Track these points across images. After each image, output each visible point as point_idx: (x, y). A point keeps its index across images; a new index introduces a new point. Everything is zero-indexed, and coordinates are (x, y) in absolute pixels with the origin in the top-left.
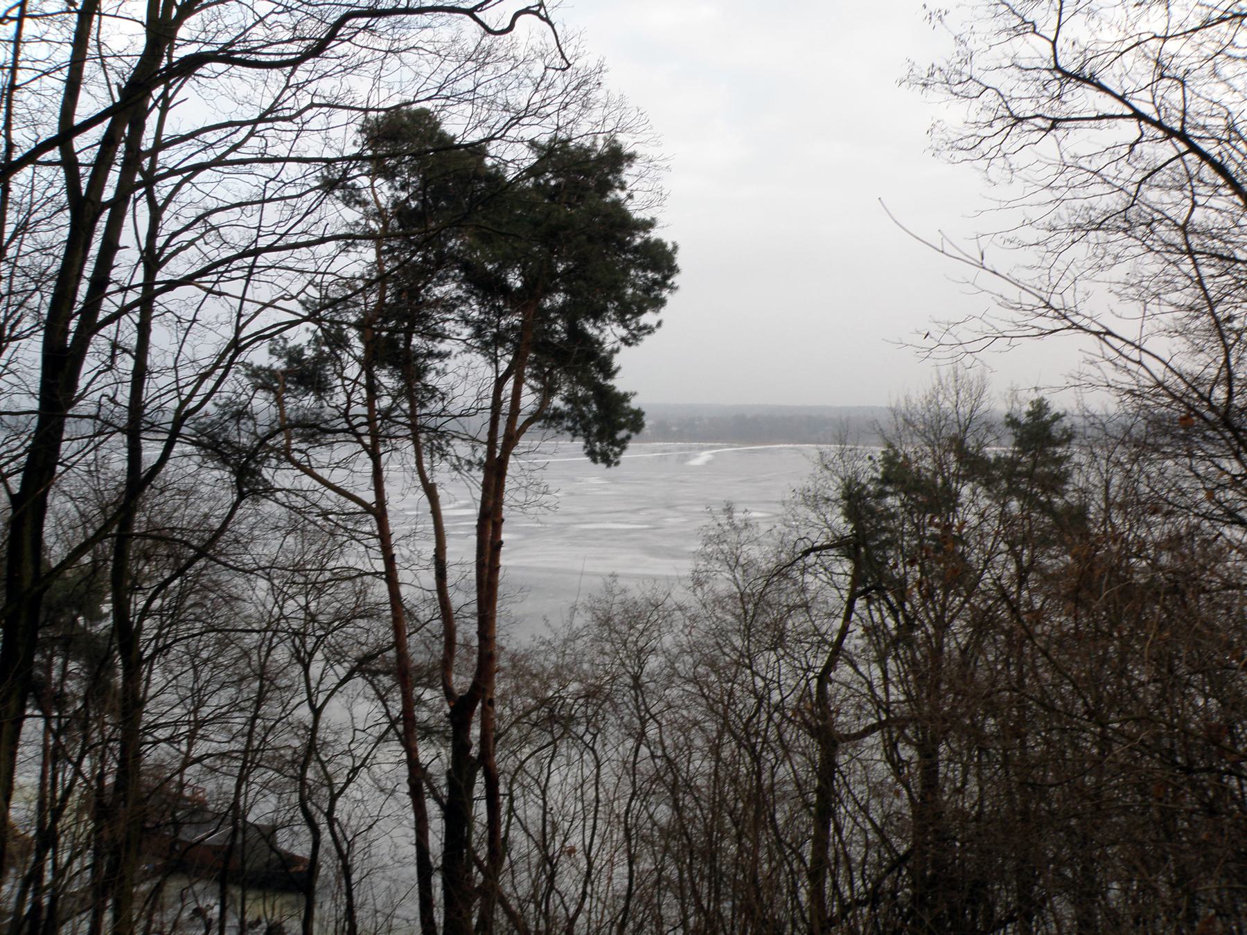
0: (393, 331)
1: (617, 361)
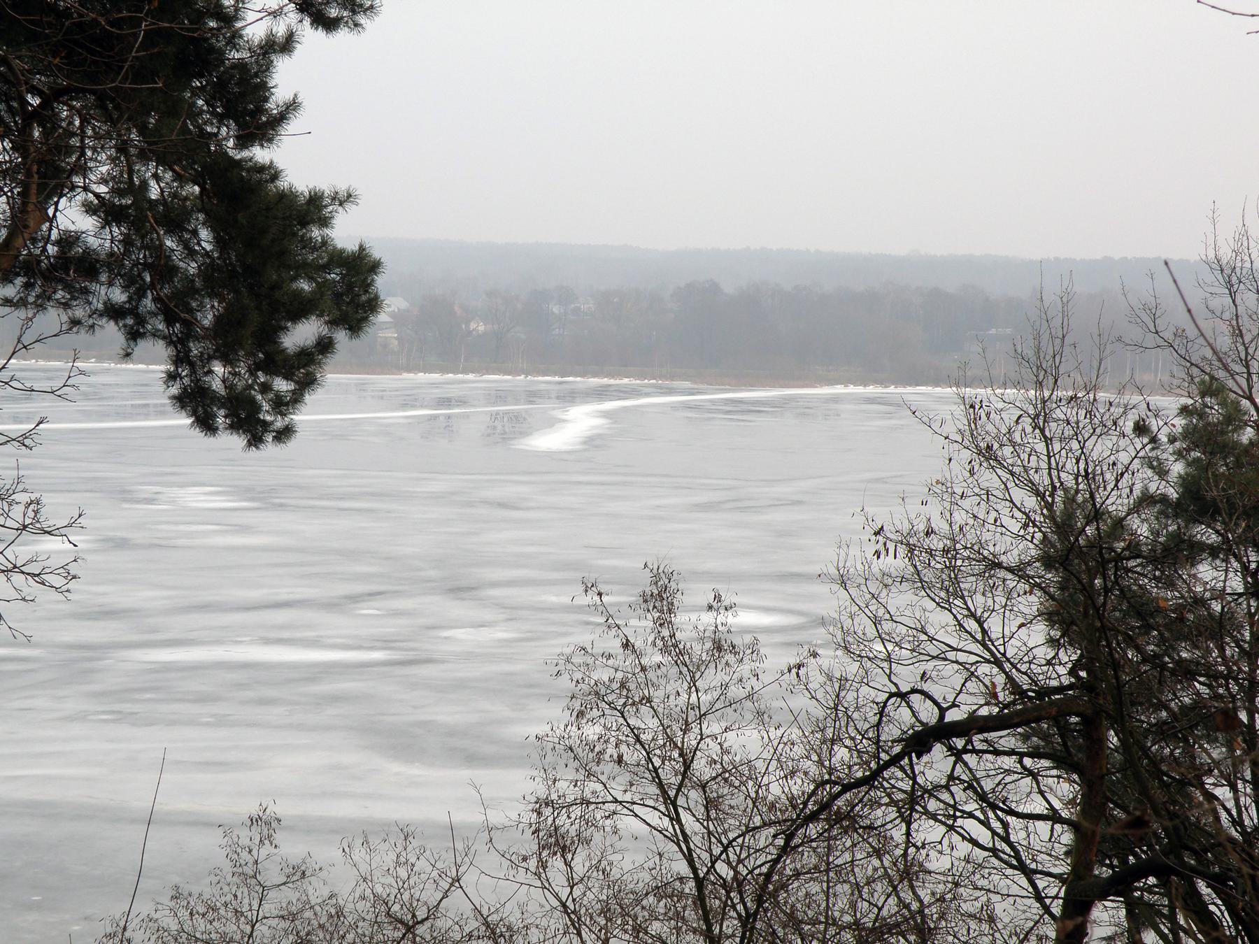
1: (285, 79)
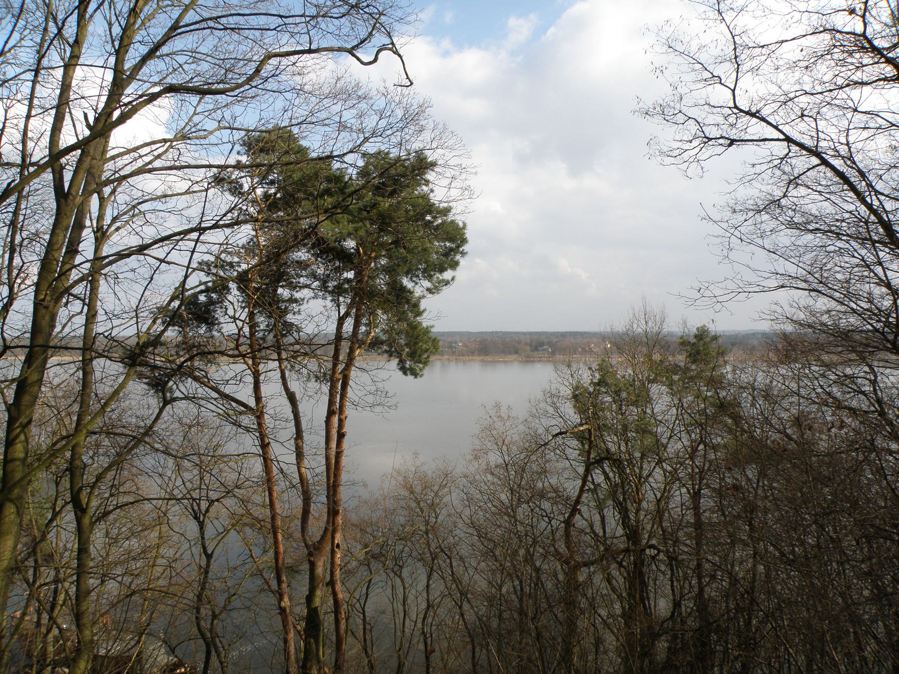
0: (266, 282)
1: (423, 305)
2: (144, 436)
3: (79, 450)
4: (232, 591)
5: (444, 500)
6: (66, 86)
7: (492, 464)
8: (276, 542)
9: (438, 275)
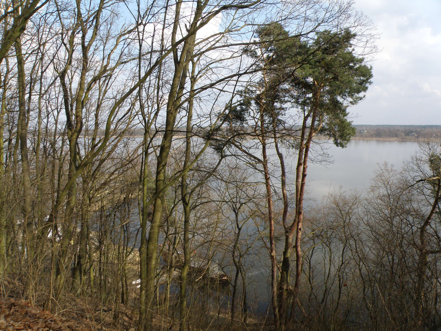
0: (268, 102)
1: (348, 110)
2: (212, 172)
3: (184, 177)
4: (249, 246)
5: (354, 211)
6: (177, 13)
7: (381, 194)
8: (271, 225)
9: (356, 94)
